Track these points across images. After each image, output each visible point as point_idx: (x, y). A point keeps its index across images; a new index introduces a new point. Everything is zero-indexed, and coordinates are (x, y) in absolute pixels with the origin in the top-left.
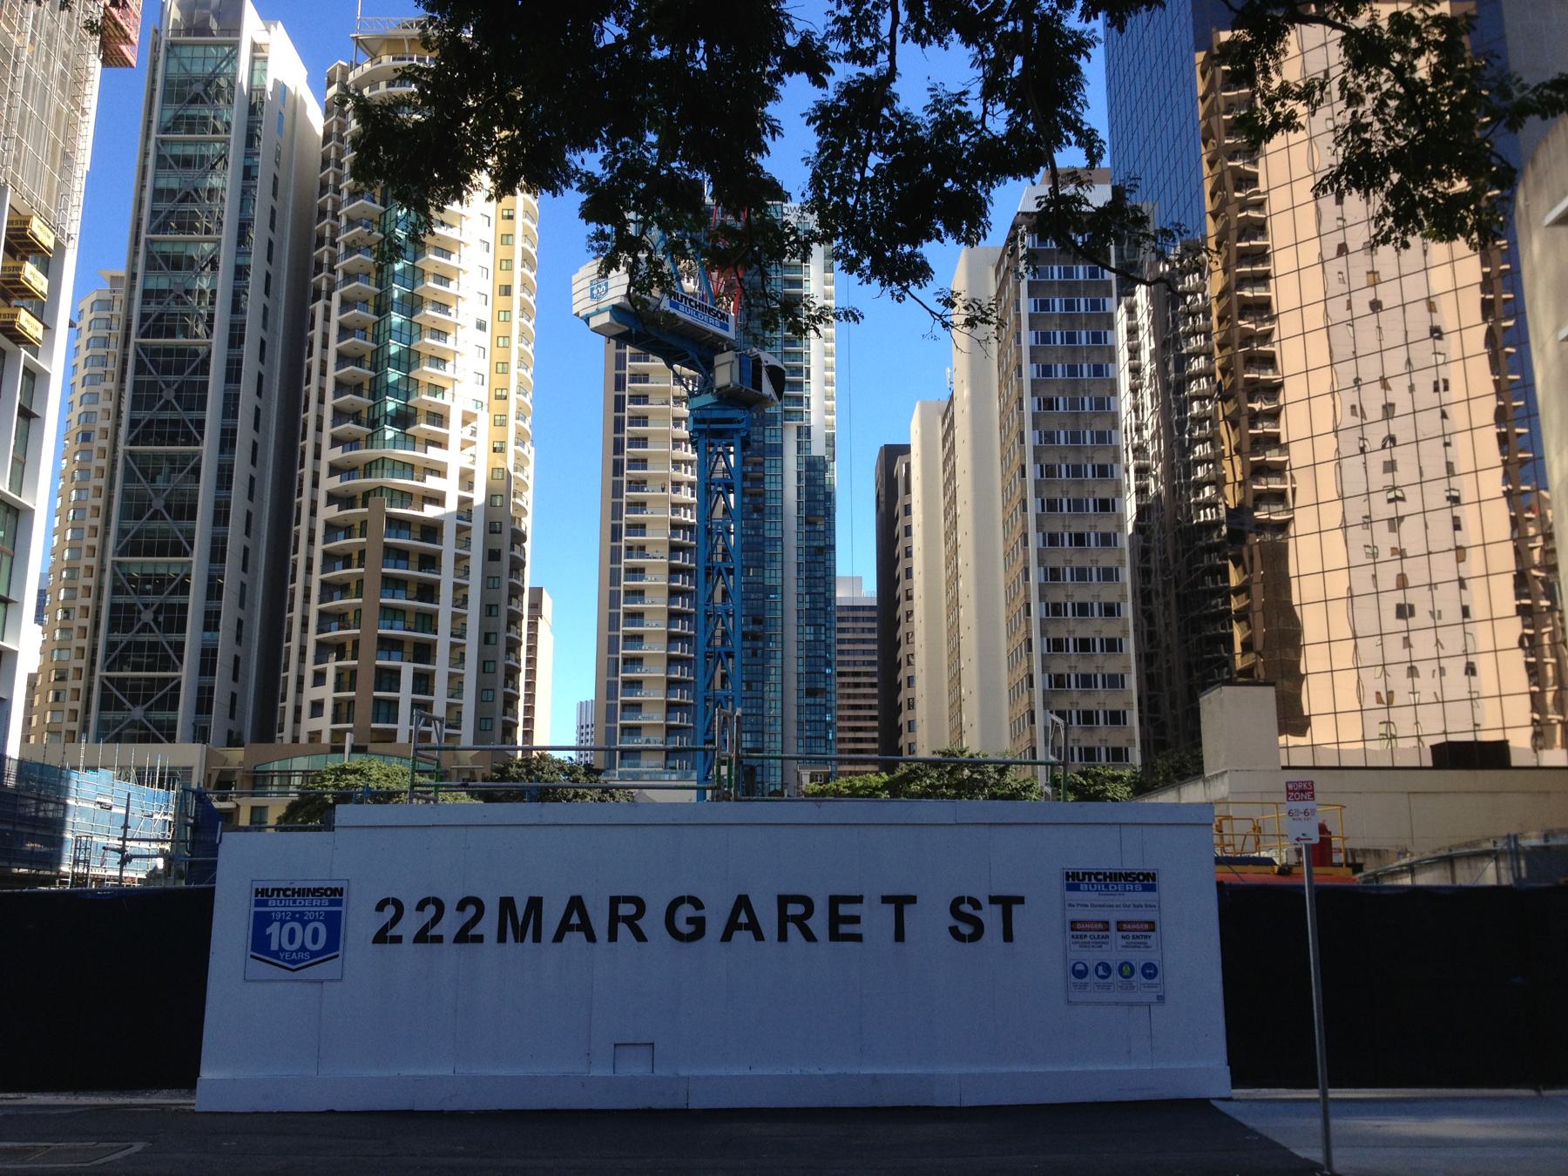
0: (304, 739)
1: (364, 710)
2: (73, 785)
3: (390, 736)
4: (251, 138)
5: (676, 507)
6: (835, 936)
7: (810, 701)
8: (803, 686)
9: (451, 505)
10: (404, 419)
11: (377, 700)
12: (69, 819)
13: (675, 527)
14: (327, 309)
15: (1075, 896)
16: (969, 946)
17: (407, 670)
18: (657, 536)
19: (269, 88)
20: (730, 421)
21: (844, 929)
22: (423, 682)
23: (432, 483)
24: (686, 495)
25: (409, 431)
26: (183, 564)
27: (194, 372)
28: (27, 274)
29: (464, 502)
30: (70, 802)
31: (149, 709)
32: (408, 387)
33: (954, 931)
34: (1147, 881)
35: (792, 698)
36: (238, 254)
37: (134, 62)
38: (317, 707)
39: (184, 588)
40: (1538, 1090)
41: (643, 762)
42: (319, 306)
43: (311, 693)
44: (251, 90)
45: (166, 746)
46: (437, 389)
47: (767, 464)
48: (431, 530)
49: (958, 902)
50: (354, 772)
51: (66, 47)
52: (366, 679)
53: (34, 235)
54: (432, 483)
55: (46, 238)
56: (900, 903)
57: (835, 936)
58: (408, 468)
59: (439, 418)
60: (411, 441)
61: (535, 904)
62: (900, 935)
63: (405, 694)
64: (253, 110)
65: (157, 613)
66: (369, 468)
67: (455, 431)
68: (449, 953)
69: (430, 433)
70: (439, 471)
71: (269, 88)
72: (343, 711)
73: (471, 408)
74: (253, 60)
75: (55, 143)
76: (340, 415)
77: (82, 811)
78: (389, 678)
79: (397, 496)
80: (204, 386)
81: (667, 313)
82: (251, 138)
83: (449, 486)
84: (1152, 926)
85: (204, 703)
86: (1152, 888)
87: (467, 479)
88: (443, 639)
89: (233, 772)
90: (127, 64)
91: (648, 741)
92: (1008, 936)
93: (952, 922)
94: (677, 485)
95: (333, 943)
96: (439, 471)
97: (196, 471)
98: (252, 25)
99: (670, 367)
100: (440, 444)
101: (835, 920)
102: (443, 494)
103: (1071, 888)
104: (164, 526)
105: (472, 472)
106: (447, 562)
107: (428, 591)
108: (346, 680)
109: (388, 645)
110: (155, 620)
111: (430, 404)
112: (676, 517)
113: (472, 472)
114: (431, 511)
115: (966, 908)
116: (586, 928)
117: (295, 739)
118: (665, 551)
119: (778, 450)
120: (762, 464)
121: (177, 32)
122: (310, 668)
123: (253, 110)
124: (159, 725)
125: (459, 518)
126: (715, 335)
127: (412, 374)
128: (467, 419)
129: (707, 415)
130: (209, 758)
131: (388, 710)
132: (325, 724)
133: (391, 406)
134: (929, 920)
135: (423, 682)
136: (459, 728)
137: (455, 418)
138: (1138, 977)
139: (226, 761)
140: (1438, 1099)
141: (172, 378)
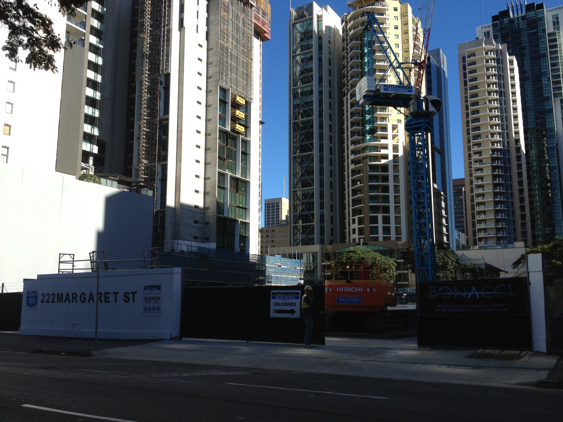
0: (351, 241)
1: (367, 231)
2: (267, 260)
3: (377, 239)
4: (320, 48)
5: (493, 143)
6: (105, 301)
9: (391, 158)
10: (373, 131)
12: (267, 270)
13: (493, 151)
14: (347, 98)
15: (145, 291)
16: (127, 303)
17: (380, 216)
18: (487, 155)
19: (324, 29)
20: (420, 123)
21: (107, 300)
22: (386, 220)
23: (383, 152)
24: (497, 138)
25: (375, 135)
26: (312, 189)
27: (309, 129)
28: (237, 114)
29: (395, 157)
30: (267, 265)
31: (307, 235)
32: (373, 120)
33: (125, 300)
34: (159, 287)
36: (319, 87)
37: (270, 38)
38: (354, 230)
39: (312, 197)
40: (248, 341)
42: (345, 98)
43: (352, 226)
44: (318, 31)
45: (312, 246)
46: (383, 119)
47: (547, 117)
48: (385, 168)
49: (126, 293)
50: (352, 252)
51: (243, 41)
52: (367, 220)
53: (238, 101)
54: (383, 152)
55: (243, 102)
56: (116, 293)
57: (105, 301)
58: (376, 148)
59: (385, 129)
60: (377, 139)
61: (62, 294)
62: (116, 301)
63: (380, 225)
64: (320, 38)
65: (306, 205)
66: (364, 149)
67: (390, 133)
68: (50, 303)
69: (381, 134)
70: (385, 147)
71: (324, 29)
72: (361, 231)
73: (395, 123)
74: (318, 21)
75: (243, 72)
76: (353, 134)
77: (271, 267)
78: (374, 220)
79: (372, 158)
80: (312, 132)
81: (384, 94)
82: (320, 48)
83: (390, 153)
84: (159, 298)
85: (322, 232)
86: (159, 289)
87: (395, 148)
88: (392, 205)
89: (330, 253)
90: (268, 39)
91: (489, 234)
92: (134, 301)
93: (124, 298)
94: (493, 135)
95: (36, 303)
96: (385, 147)
97: (313, 159)
98: (317, 9)
99: (396, 109)
100: (385, 138)
101: (106, 298)
102: (388, 155)
103: (145, 289)
104: (306, 178)
105: (398, 145)
106: (391, 178)
107: (386, 189)
108: (361, 222)
109: (374, 209)
110: (306, 207)
111: (381, 124)
112: (493, 147)
113: (398, 145)
114: (383, 161)
115: (127, 295)
116: (69, 300)
117: (350, 241)
118: (490, 160)
119: (551, 111)
120: (544, 118)
121: (295, 19)
122: (351, 218)
123: (320, 38)
124: (310, 239)
125: (394, 162)
126: (406, 95)
127: (374, 116)
128: (394, 127)
129: (411, 123)
130: (322, 249)
131: (375, 230)
132: (356, 236)
133: (368, 128)
134: (121, 297)
135: (386, 220)
137: (390, 128)
138: (156, 311)
139: (327, 250)
140: (258, 344)
141: (304, 131)
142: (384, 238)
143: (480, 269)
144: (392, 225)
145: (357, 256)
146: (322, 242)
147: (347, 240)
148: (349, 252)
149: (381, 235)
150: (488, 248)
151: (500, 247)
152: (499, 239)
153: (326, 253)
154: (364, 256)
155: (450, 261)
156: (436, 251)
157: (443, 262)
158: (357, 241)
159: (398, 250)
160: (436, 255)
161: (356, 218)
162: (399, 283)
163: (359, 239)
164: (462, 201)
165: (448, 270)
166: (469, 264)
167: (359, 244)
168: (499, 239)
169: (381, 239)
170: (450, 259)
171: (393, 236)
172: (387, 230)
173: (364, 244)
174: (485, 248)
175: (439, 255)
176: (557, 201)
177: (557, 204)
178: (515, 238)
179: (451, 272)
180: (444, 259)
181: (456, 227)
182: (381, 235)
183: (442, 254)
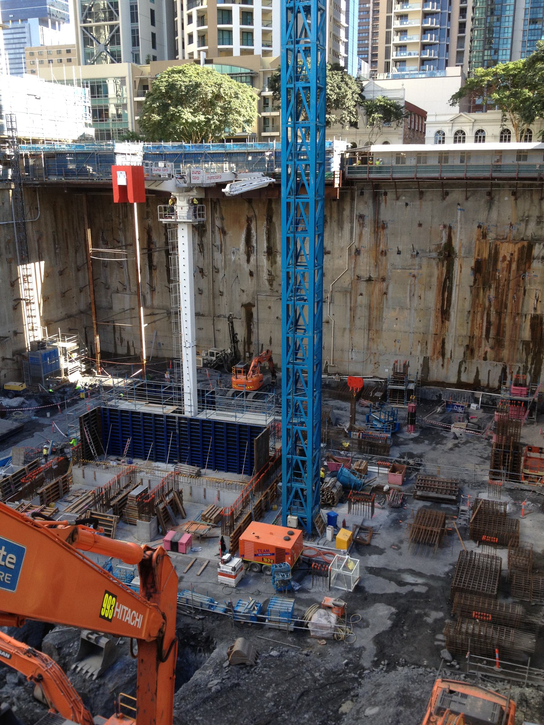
0: (187, 57)
1: (213, 37)
3: (229, 52)
7: (532, 27)
8: (528, 17)
11: (220, 30)
35: (520, 25)
41: (407, 68)
50: (179, 72)
52: (212, 17)
63: (236, 26)
85: (460, 54)
91: (410, 54)
108: (202, 20)
117: (184, 58)
122: (186, 12)
131: (226, 36)
132: (193, 48)
136: (270, 46)
142: (243, 52)
143: (397, 107)
144: (257, 27)
145: (187, 80)
146: (136, 59)
147: (180, 56)
148: (173, 72)
149: (236, 46)
150: (406, 77)
151: (424, 76)
152: (423, 62)
153: (142, 80)
154: (199, 80)
155: (349, 92)
156: (328, 73)
157: (338, 94)
158: (196, 57)
159: (264, 73)
160: (328, 80)
161: (194, 11)
162: (263, 134)
163: (199, 52)
164: (368, 12)
165: (344, 109)
166: (380, 97)
167: (198, 62)
168: (423, 62)
169: (236, 53)
170: (350, 88)
171: (258, 47)
172: (247, 37)
173: (207, 62)
174: (402, 77)
175: (333, 80)
176: (508, 8)
177: (507, 13)
178: (447, 61)
179: (351, 112)
180: (340, 89)
181: (359, 53)
182: (236, 46)
183: (338, 78)
